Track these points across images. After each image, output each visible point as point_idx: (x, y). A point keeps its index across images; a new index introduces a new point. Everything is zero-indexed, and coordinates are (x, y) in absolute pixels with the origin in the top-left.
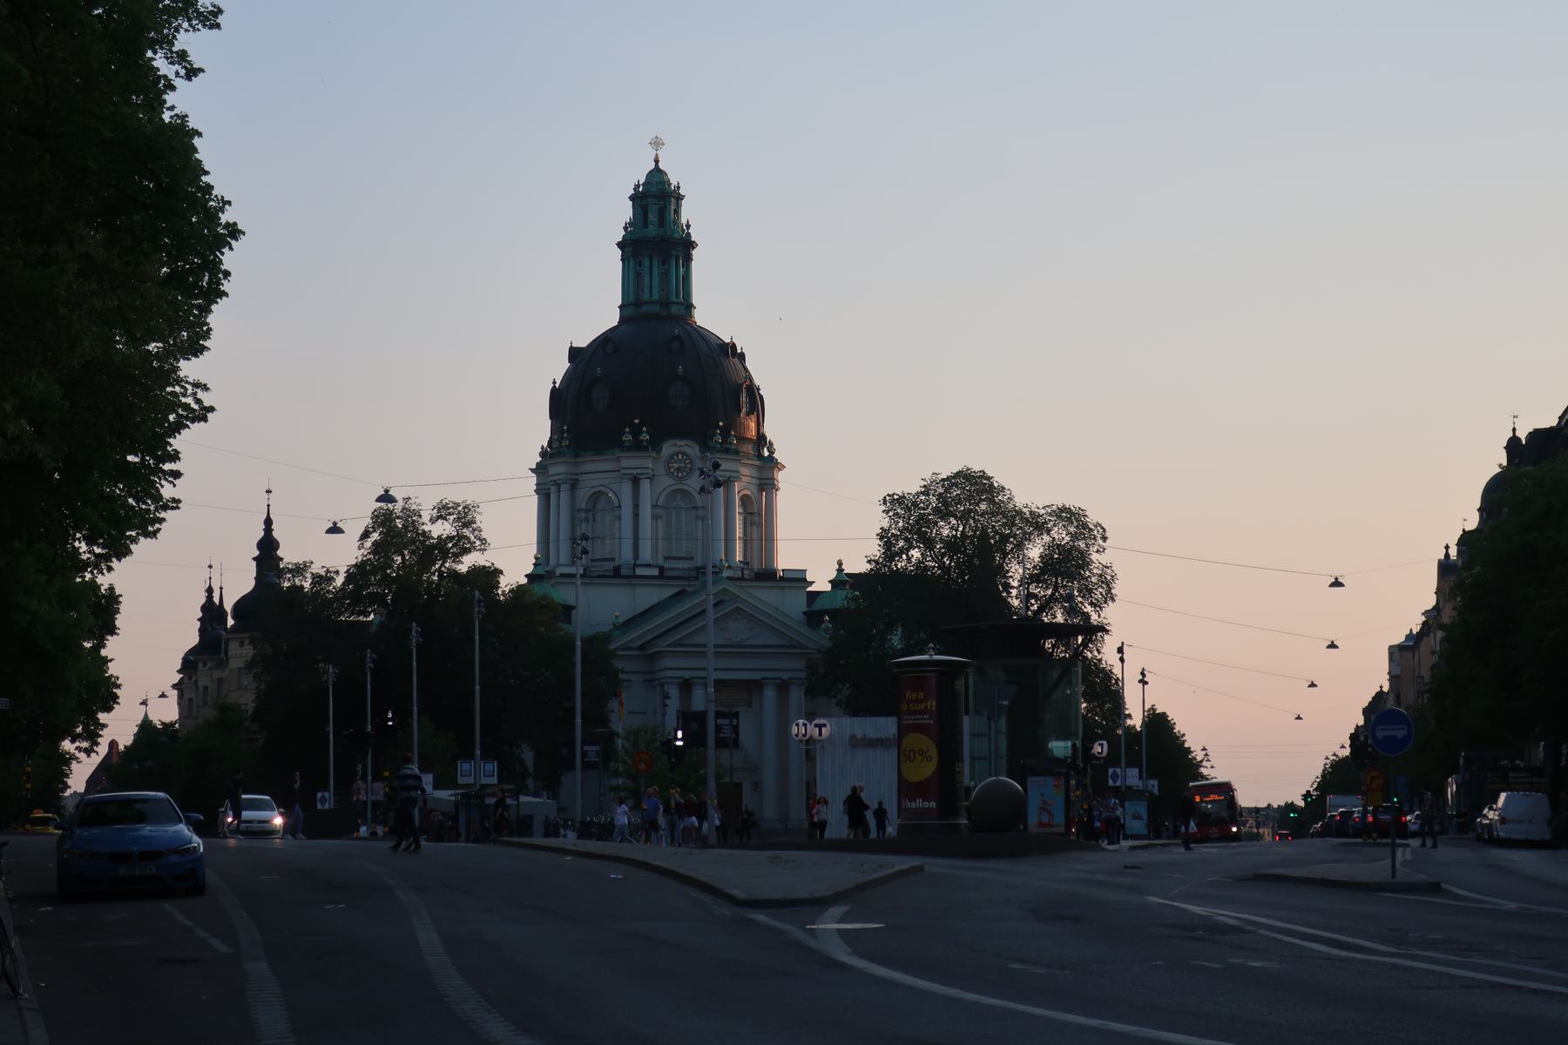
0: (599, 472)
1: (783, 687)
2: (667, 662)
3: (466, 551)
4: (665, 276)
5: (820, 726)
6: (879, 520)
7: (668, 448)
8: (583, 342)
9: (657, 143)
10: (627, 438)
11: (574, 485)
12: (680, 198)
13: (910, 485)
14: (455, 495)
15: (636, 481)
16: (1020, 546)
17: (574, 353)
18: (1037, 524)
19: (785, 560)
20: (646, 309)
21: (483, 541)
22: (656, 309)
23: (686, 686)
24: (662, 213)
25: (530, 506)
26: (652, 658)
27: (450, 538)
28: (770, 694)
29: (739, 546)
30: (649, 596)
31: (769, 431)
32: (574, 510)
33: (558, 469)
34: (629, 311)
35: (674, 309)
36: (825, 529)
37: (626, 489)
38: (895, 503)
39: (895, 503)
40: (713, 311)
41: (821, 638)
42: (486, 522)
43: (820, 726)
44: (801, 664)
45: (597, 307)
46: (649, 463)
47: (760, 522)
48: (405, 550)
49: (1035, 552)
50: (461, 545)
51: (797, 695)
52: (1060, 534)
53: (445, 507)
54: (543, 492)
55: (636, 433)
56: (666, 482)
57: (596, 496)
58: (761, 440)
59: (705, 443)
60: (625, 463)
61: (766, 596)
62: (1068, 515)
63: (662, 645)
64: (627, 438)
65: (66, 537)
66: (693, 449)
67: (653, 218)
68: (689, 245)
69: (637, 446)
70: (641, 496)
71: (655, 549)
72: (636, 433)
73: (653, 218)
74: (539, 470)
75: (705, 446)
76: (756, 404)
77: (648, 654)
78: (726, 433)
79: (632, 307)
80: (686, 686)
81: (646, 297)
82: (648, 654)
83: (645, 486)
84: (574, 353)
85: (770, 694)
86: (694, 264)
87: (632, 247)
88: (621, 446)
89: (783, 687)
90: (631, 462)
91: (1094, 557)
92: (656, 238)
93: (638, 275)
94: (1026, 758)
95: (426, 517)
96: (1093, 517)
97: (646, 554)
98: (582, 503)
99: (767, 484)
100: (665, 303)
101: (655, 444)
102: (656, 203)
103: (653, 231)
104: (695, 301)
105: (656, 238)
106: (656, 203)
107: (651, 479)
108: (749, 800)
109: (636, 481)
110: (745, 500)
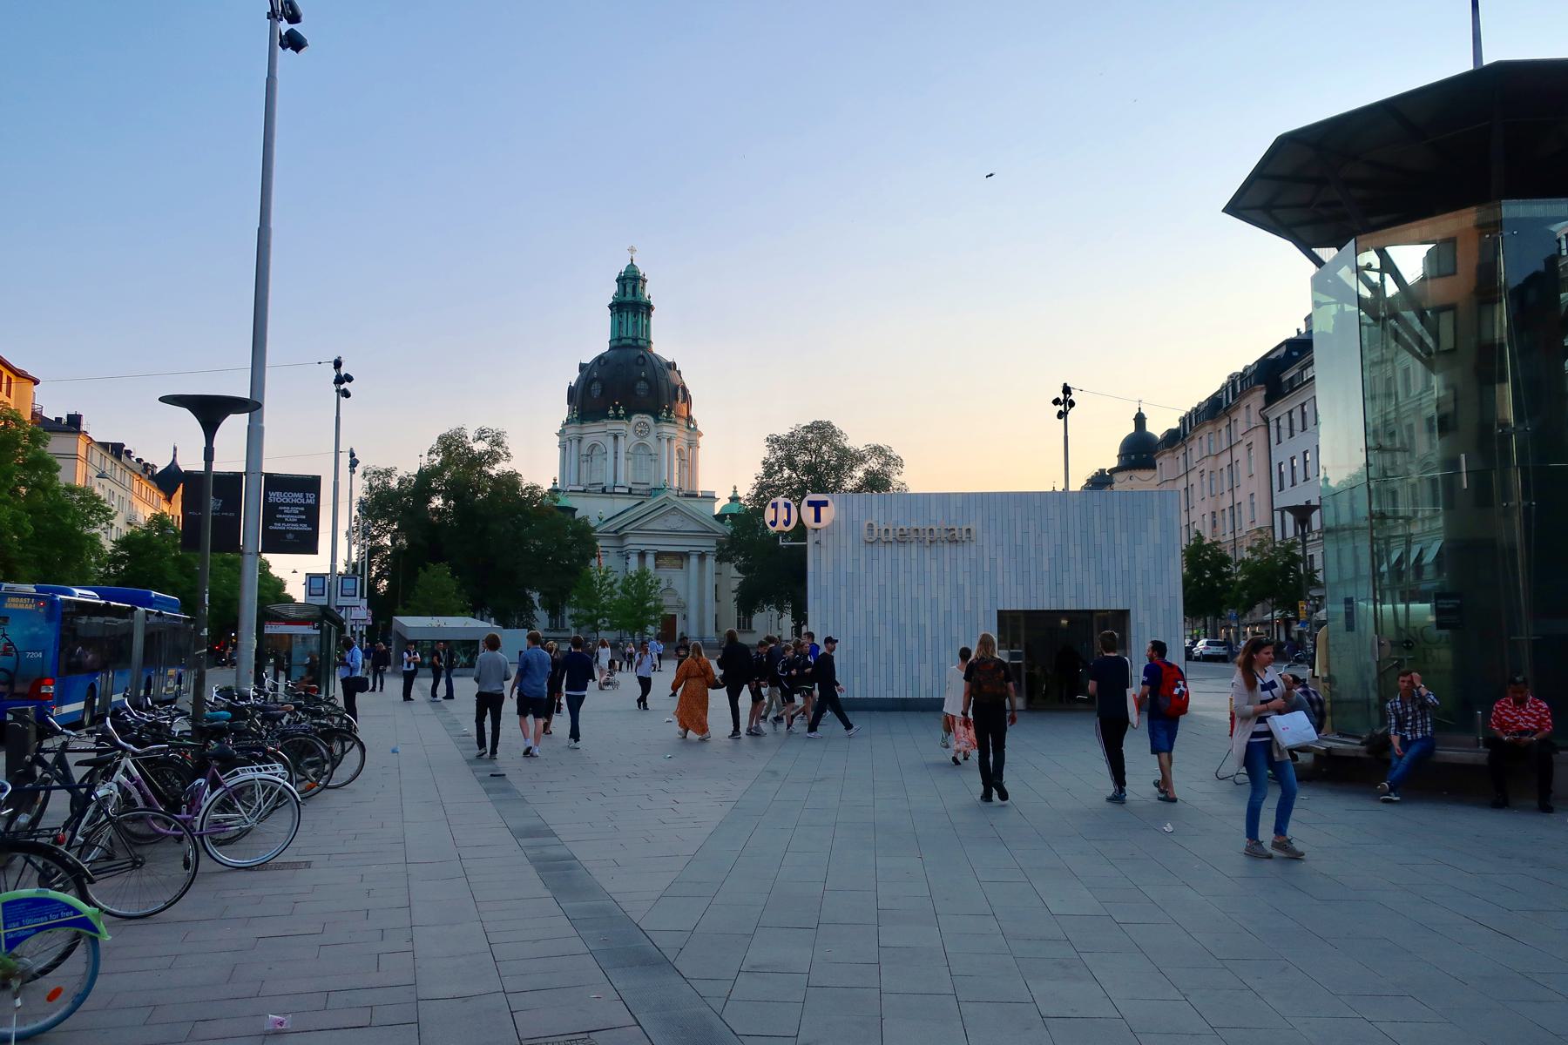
0: (596, 432)
1: (702, 556)
2: (631, 540)
3: (496, 461)
4: (635, 324)
5: (817, 506)
6: (763, 452)
7: (636, 418)
8: (587, 361)
9: (632, 250)
10: (611, 412)
12: (645, 281)
13: (783, 431)
14: (493, 425)
15: (616, 437)
16: (851, 469)
17: (582, 367)
18: (860, 459)
19: (703, 486)
21: (508, 455)
23: (642, 555)
24: (634, 288)
25: (556, 453)
26: (622, 538)
27: (487, 452)
28: (694, 560)
29: (676, 477)
30: (622, 504)
31: (693, 413)
32: (580, 455)
33: (572, 431)
35: (641, 342)
36: (727, 462)
37: (611, 439)
38: (774, 441)
39: (774, 441)
40: (663, 344)
41: (727, 529)
42: (510, 443)
43: (817, 506)
44: (713, 543)
45: (596, 340)
47: (688, 463)
48: (461, 468)
49: (859, 473)
50: (494, 457)
51: (710, 562)
52: (874, 464)
53: (483, 431)
54: (563, 446)
55: (616, 409)
56: (633, 439)
58: (689, 419)
59: (657, 417)
61: (693, 504)
62: (878, 451)
63: (627, 530)
64: (611, 412)
66: (649, 419)
67: (629, 290)
68: (649, 308)
69: (617, 417)
71: (626, 477)
72: (616, 409)
73: (629, 290)
74: (561, 433)
75: (657, 420)
76: (687, 399)
77: (619, 535)
78: (669, 411)
79: (618, 343)
80: (642, 555)
82: (619, 535)
83: (621, 439)
84: (582, 367)
85: (694, 560)
87: (617, 307)
88: (607, 417)
89: (702, 556)
91: (896, 477)
92: (630, 303)
94: (147, 693)
95: (470, 439)
96: (896, 452)
97: (621, 481)
99: (693, 445)
100: (636, 339)
101: (628, 416)
102: (630, 281)
103: (629, 297)
105: (630, 303)
106: (630, 281)
108: (680, 628)
109: (616, 437)
110: (680, 451)
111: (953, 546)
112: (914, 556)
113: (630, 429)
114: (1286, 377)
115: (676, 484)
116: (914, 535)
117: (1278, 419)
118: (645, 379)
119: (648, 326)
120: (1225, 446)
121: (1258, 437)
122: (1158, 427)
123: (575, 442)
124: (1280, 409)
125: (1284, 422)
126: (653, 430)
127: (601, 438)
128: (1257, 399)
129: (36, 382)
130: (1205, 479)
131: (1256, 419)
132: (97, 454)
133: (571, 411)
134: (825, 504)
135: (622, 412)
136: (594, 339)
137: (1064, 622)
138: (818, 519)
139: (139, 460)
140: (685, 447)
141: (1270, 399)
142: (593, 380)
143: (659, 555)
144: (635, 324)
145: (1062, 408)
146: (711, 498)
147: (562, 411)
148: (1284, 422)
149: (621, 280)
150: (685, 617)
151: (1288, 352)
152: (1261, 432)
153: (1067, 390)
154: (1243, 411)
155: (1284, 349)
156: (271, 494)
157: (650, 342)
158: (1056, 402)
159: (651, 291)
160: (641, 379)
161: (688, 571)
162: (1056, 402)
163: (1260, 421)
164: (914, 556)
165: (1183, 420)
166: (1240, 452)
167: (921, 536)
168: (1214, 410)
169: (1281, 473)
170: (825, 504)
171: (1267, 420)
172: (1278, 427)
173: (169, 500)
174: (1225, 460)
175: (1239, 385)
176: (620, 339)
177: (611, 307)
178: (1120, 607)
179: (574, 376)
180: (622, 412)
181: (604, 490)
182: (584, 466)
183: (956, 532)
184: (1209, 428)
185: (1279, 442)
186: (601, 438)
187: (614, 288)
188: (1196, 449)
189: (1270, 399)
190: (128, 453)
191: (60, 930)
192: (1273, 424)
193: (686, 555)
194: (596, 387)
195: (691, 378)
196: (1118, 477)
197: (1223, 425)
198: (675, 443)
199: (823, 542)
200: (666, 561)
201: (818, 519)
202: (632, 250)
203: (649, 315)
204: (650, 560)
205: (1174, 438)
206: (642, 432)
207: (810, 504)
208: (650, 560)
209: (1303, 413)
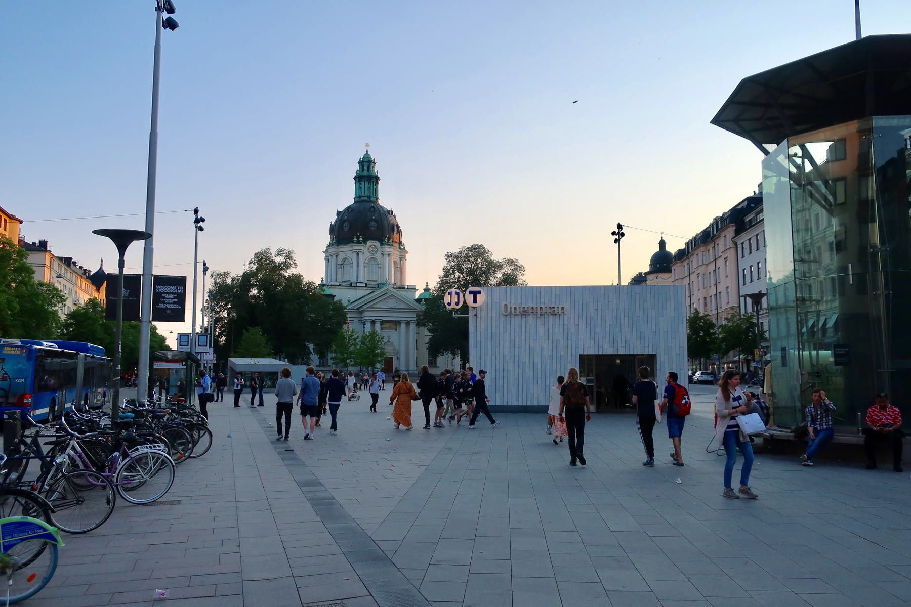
0: (346, 251)
1: (408, 323)
2: (367, 314)
3: (288, 268)
4: (369, 188)
5: (475, 294)
6: (443, 263)
7: (369, 243)
8: (341, 210)
9: (367, 145)
10: (355, 239)
12: (374, 163)
13: (455, 250)
14: (286, 247)
15: (358, 254)
16: (494, 272)
17: (338, 213)
18: (499, 266)
19: (408, 282)
21: (295, 264)
23: (373, 322)
24: (369, 167)
25: (323, 263)
26: (361, 312)
27: (283, 263)
28: (403, 325)
29: (393, 277)
30: (361, 293)
31: (403, 240)
32: (337, 264)
33: (333, 250)
35: (372, 199)
36: (422, 269)
37: (355, 255)
38: (449, 256)
39: (449, 256)
40: (385, 200)
41: (422, 307)
42: (296, 257)
43: (475, 294)
44: (415, 315)
45: (346, 198)
47: (400, 269)
48: (268, 272)
49: (499, 275)
50: (287, 266)
51: (413, 326)
52: (508, 269)
53: (281, 251)
54: (327, 259)
55: (358, 238)
56: (368, 255)
58: (400, 243)
59: (382, 242)
61: (402, 293)
62: (510, 262)
63: (364, 308)
64: (355, 239)
66: (377, 244)
67: (366, 168)
68: (377, 179)
69: (359, 242)
71: (364, 277)
72: (358, 238)
73: (366, 168)
74: (326, 252)
75: (382, 244)
76: (399, 232)
77: (360, 311)
78: (389, 239)
79: (359, 199)
80: (373, 322)
82: (360, 311)
83: (361, 255)
84: (338, 213)
85: (403, 325)
87: (359, 178)
88: (353, 242)
89: (408, 323)
91: (521, 277)
92: (366, 176)
94: (86, 403)
95: (273, 255)
96: (521, 263)
97: (361, 279)
99: (402, 258)
100: (369, 197)
101: (365, 242)
102: (366, 163)
103: (365, 173)
105: (366, 176)
106: (366, 163)
108: (395, 365)
109: (358, 254)
110: (395, 262)
111: (554, 317)
112: (531, 323)
113: (366, 249)
114: (747, 219)
115: (393, 281)
116: (531, 311)
117: (742, 244)
118: (375, 220)
119: (376, 189)
120: (712, 259)
121: (731, 254)
122: (673, 248)
123: (334, 257)
124: (744, 237)
125: (746, 245)
126: (379, 250)
127: (349, 254)
128: (730, 231)
129: (21, 222)
130: (700, 278)
131: (730, 244)
132: (56, 264)
133: (332, 239)
134: (479, 293)
135: (361, 239)
136: (345, 197)
137: (618, 361)
138: (475, 301)
139: (81, 267)
140: (398, 260)
141: (738, 232)
142: (345, 221)
143: (383, 323)
144: (369, 188)
145: (617, 237)
146: (413, 289)
147: (326, 238)
148: (746, 245)
149: (361, 163)
150: (398, 358)
151: (748, 205)
152: (733, 251)
153: (620, 226)
154: (722, 239)
155: (746, 203)
156: (158, 287)
157: (377, 199)
158: (614, 233)
159: (378, 169)
160: (373, 220)
161: (400, 332)
162: (614, 233)
163: (732, 245)
164: (531, 323)
165: (687, 244)
166: (720, 262)
167: (535, 311)
168: (705, 238)
169: (744, 275)
170: (479, 293)
171: (736, 244)
172: (743, 248)
173: (98, 290)
174: (712, 267)
175: (720, 224)
176: (360, 197)
177: (355, 178)
178: (651, 353)
179: (333, 218)
180: (361, 239)
181: (351, 285)
182: (340, 271)
183: (556, 309)
184: (702, 249)
185: (743, 257)
186: (349, 254)
187: (357, 167)
188: (695, 261)
189: (738, 232)
190: (75, 263)
191: (35, 540)
192: (740, 247)
193: (399, 323)
194: (346, 225)
195: (401, 219)
197: (710, 247)
198: (392, 257)
199: (478, 315)
200: (387, 326)
201: (475, 301)
202: (367, 145)
203: (377, 183)
204: (378, 325)
205: (682, 255)
206: (373, 251)
207: (471, 292)
208: (378, 325)
209: (757, 240)
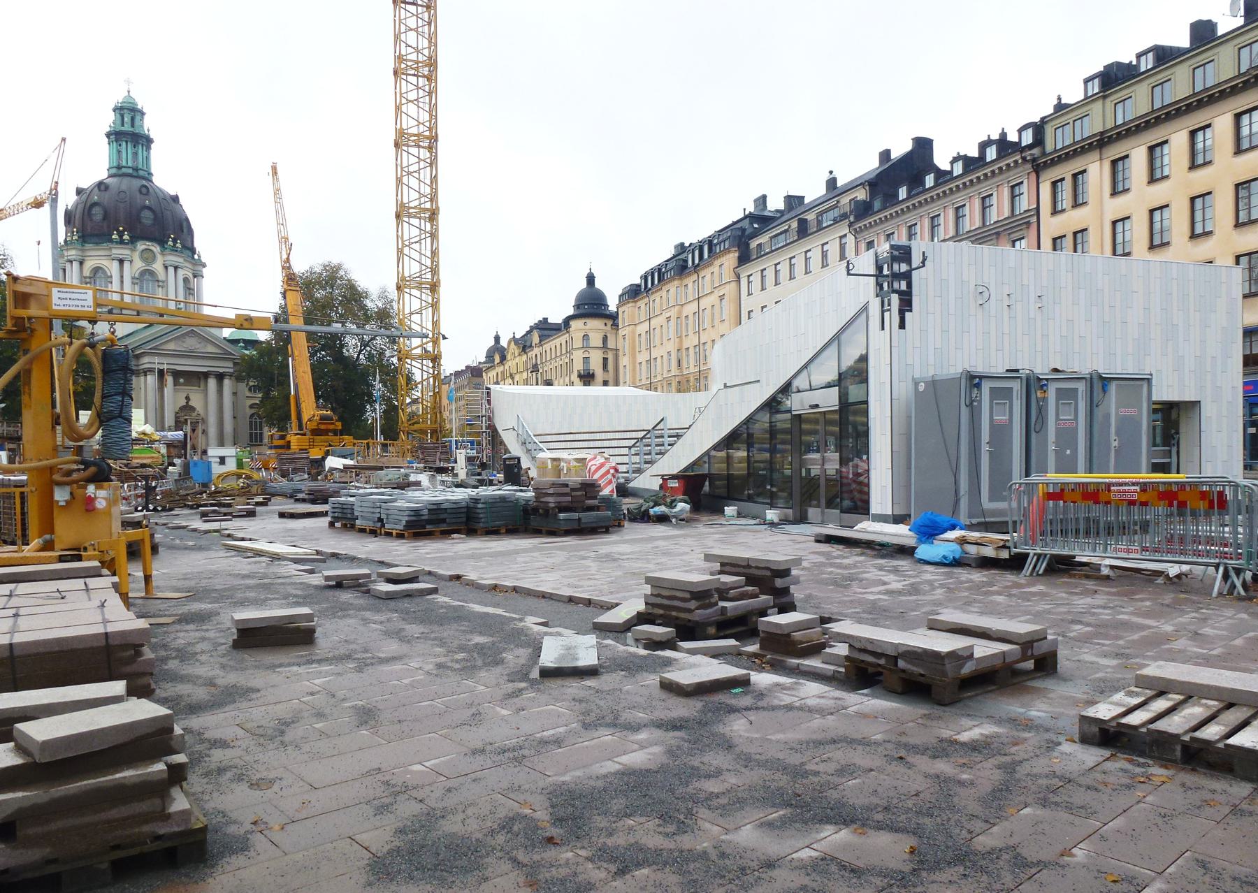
1: (220, 377)
4: (135, 154)
7: (141, 246)
9: (128, 82)
11: (81, 263)
15: (121, 262)
20: (124, 170)
22: (130, 171)
24: (133, 119)
28: (212, 383)
34: (114, 171)
37: (116, 264)
40: (168, 173)
46: (127, 252)
55: (121, 234)
56: (139, 264)
57: (96, 270)
60: (114, 251)
65: (899, 185)
66: (156, 249)
69: (122, 242)
70: (122, 269)
72: (121, 234)
79: (118, 171)
81: (124, 164)
83: (126, 265)
85: (212, 383)
86: (152, 152)
87: (116, 136)
88: (111, 241)
89: (176, 268)
90: (123, 252)
93: (119, 152)
98: (87, 273)
101: (133, 240)
102: (129, 112)
103: (127, 128)
104: (153, 171)
106: (129, 112)
107: (131, 262)
109: (121, 262)
110: (186, 280)
119: (148, 158)
121: (730, 289)
124: (753, 269)
126: (159, 257)
127: (104, 263)
128: (731, 259)
130: (672, 323)
135: (126, 237)
141: (744, 259)
142: (95, 204)
144: (135, 154)
152: (733, 285)
156: (875, 508)
159: (150, 125)
165: (645, 278)
171: (738, 277)
176: (119, 167)
177: (108, 135)
180: (126, 237)
184: (676, 283)
186: (104, 263)
189: (744, 259)
192: (744, 281)
193: (206, 375)
195: (191, 208)
196: (575, 324)
198: (180, 272)
202: (128, 82)
203: (149, 148)
206: (148, 257)
